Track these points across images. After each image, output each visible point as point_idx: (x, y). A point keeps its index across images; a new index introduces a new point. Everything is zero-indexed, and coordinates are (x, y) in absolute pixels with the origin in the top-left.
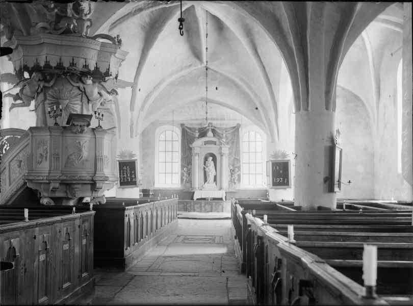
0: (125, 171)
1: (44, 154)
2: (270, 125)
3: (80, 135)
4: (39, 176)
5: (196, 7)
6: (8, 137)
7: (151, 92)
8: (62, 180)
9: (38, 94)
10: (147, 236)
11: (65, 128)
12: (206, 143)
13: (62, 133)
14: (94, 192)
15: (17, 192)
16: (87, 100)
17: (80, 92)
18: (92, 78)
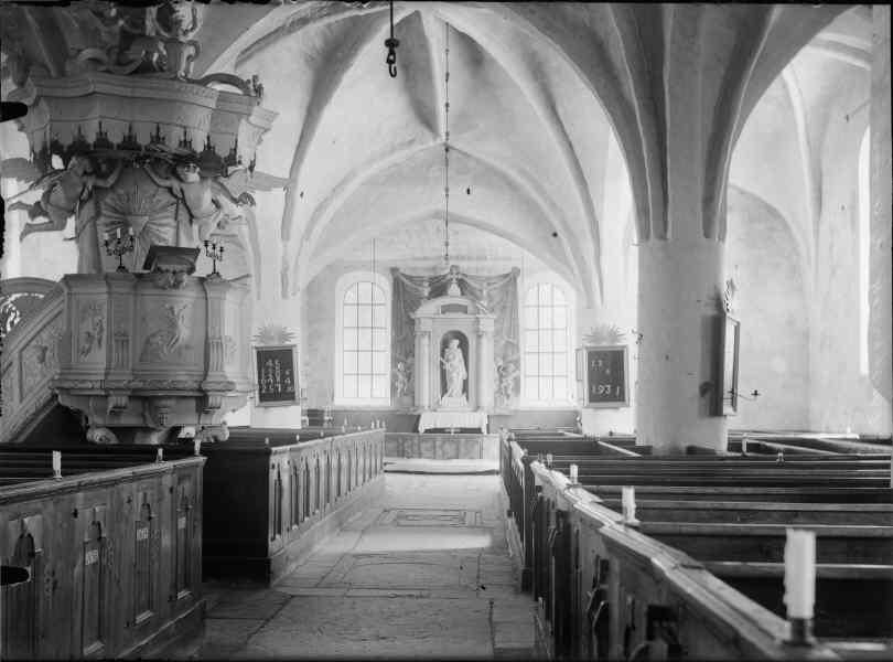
0: (270, 370)
1: (96, 334)
2: (583, 270)
3: (174, 292)
4: (84, 381)
5: (423, 15)
6: (18, 295)
7: (326, 200)
8: (135, 390)
9: (83, 203)
10: (317, 511)
11: (139, 276)
12: (446, 309)
13: (135, 287)
14: (203, 416)
15: (36, 414)
16: (188, 216)
17: (174, 200)
18: (198, 169)
